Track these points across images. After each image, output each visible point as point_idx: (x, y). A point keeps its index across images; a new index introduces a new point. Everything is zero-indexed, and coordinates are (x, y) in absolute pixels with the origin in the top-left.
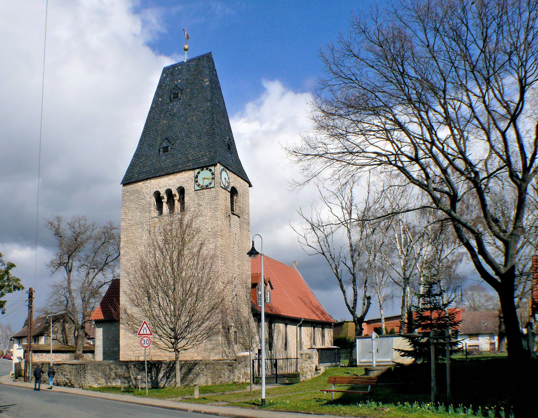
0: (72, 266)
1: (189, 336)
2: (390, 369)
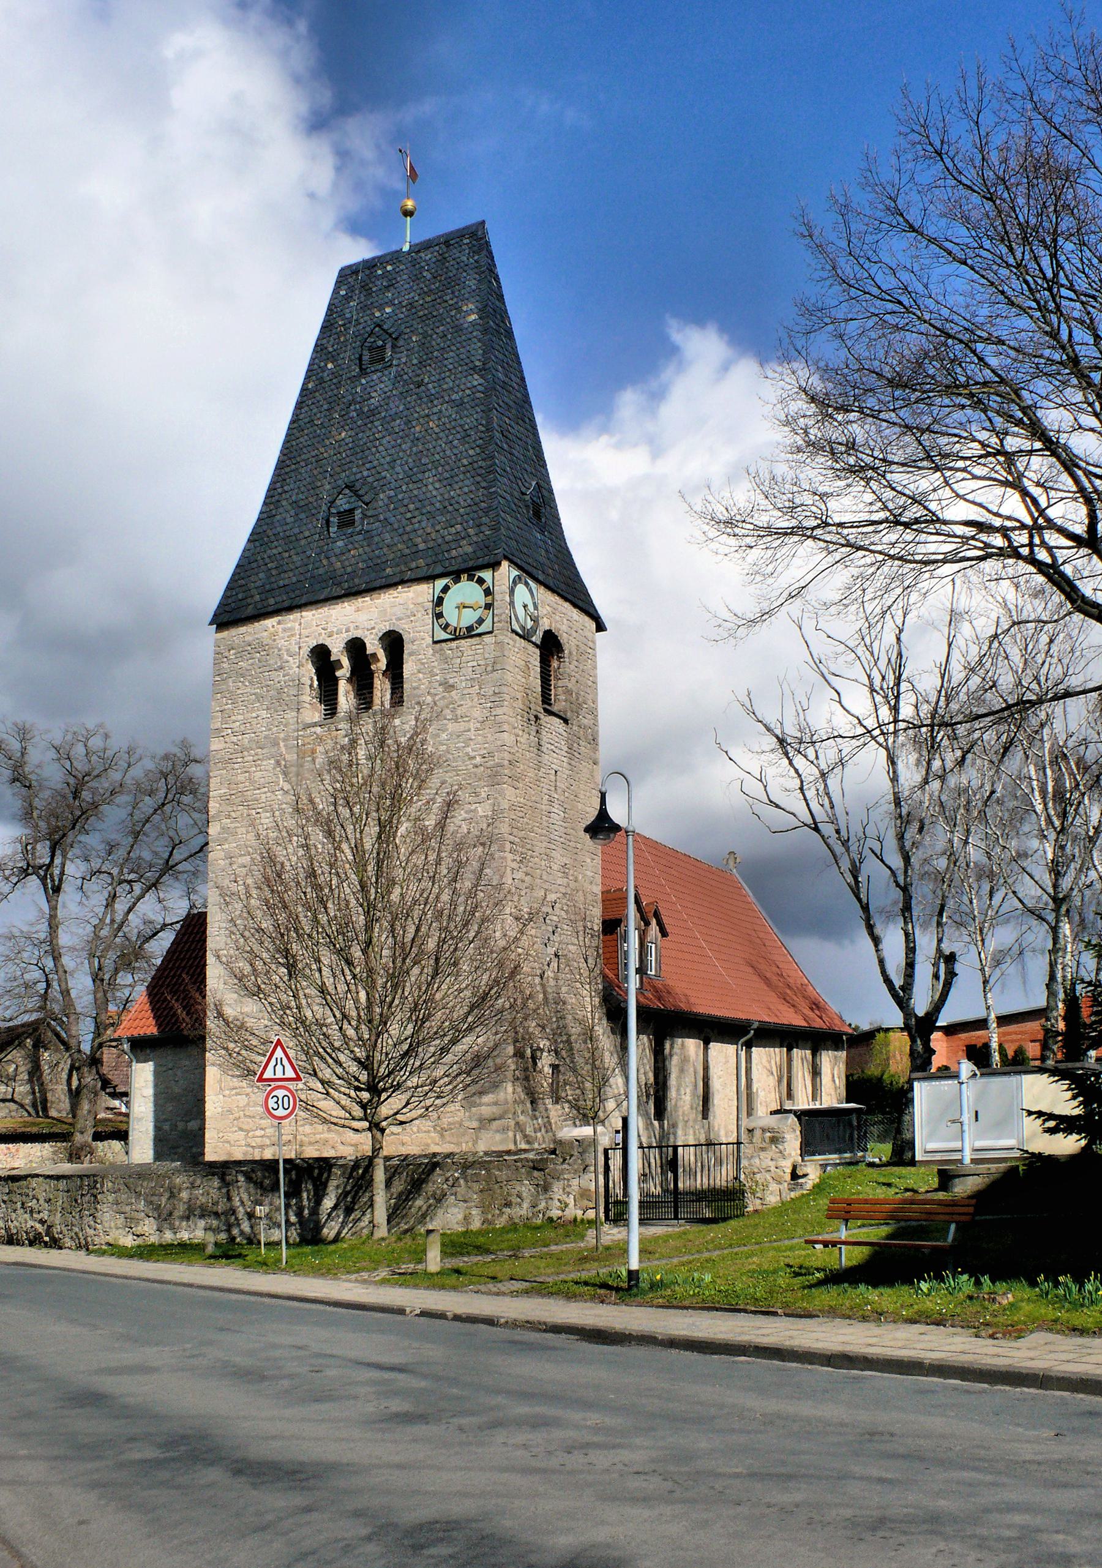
0: (62, 873)
1: (414, 1081)
2: (1014, 1170)
